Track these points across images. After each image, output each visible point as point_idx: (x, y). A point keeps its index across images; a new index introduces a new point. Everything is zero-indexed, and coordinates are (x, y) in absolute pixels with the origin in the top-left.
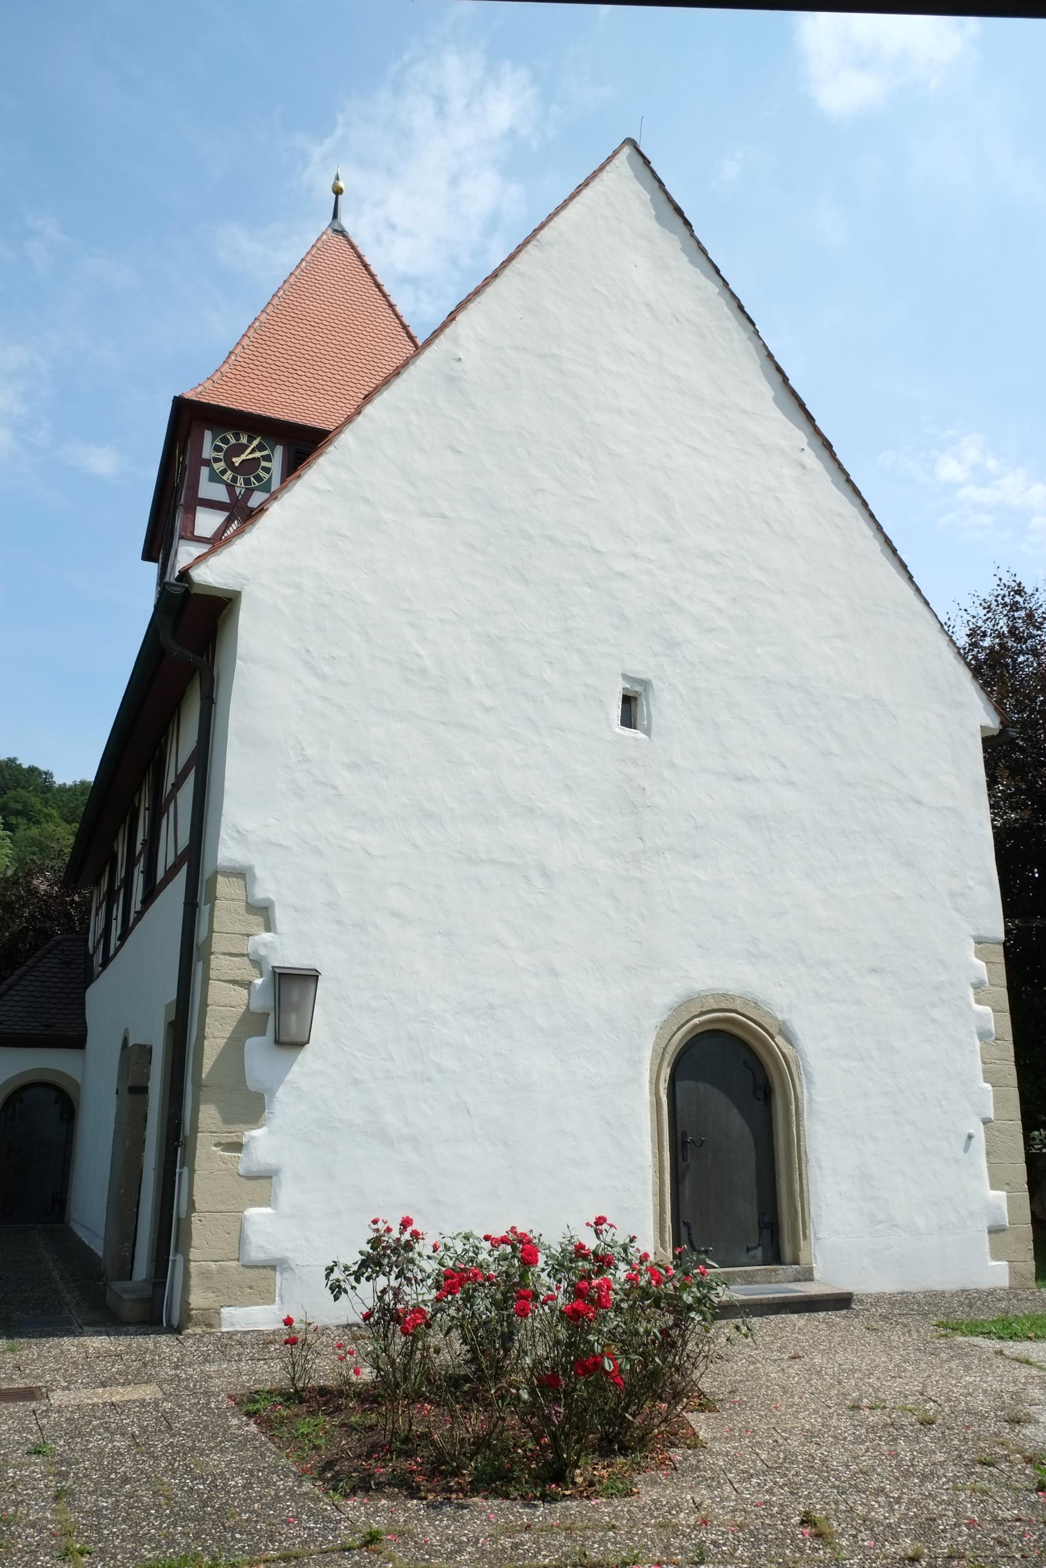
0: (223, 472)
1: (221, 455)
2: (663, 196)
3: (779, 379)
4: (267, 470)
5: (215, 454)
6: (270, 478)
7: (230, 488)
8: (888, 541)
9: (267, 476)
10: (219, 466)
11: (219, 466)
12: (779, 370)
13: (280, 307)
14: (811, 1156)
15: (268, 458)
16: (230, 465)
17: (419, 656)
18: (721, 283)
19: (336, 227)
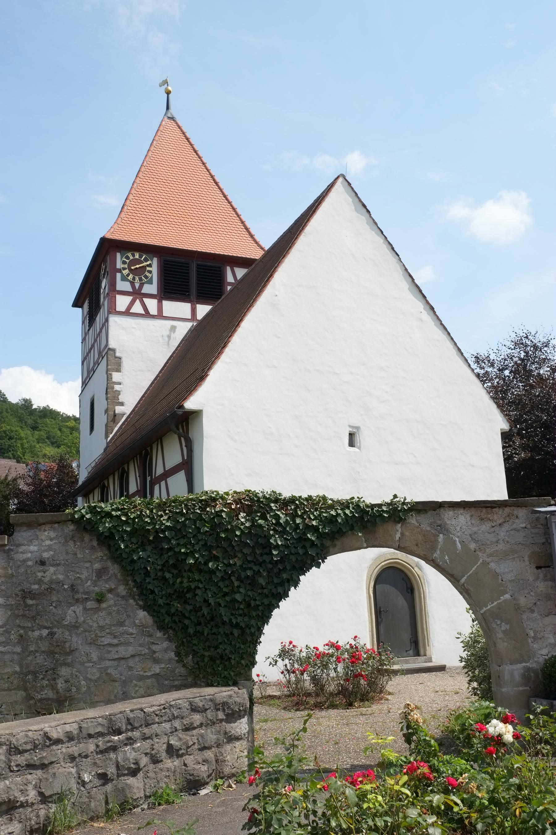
0: (128, 275)
1: (126, 266)
2: (357, 200)
3: (410, 280)
4: (150, 272)
5: (123, 266)
6: (152, 276)
7: (132, 284)
8: (459, 350)
9: (150, 275)
10: (126, 272)
11: (126, 272)
12: (410, 276)
13: (145, 172)
14: (430, 614)
15: (150, 265)
16: (131, 270)
17: (270, 428)
18: (384, 238)
19: (169, 115)
